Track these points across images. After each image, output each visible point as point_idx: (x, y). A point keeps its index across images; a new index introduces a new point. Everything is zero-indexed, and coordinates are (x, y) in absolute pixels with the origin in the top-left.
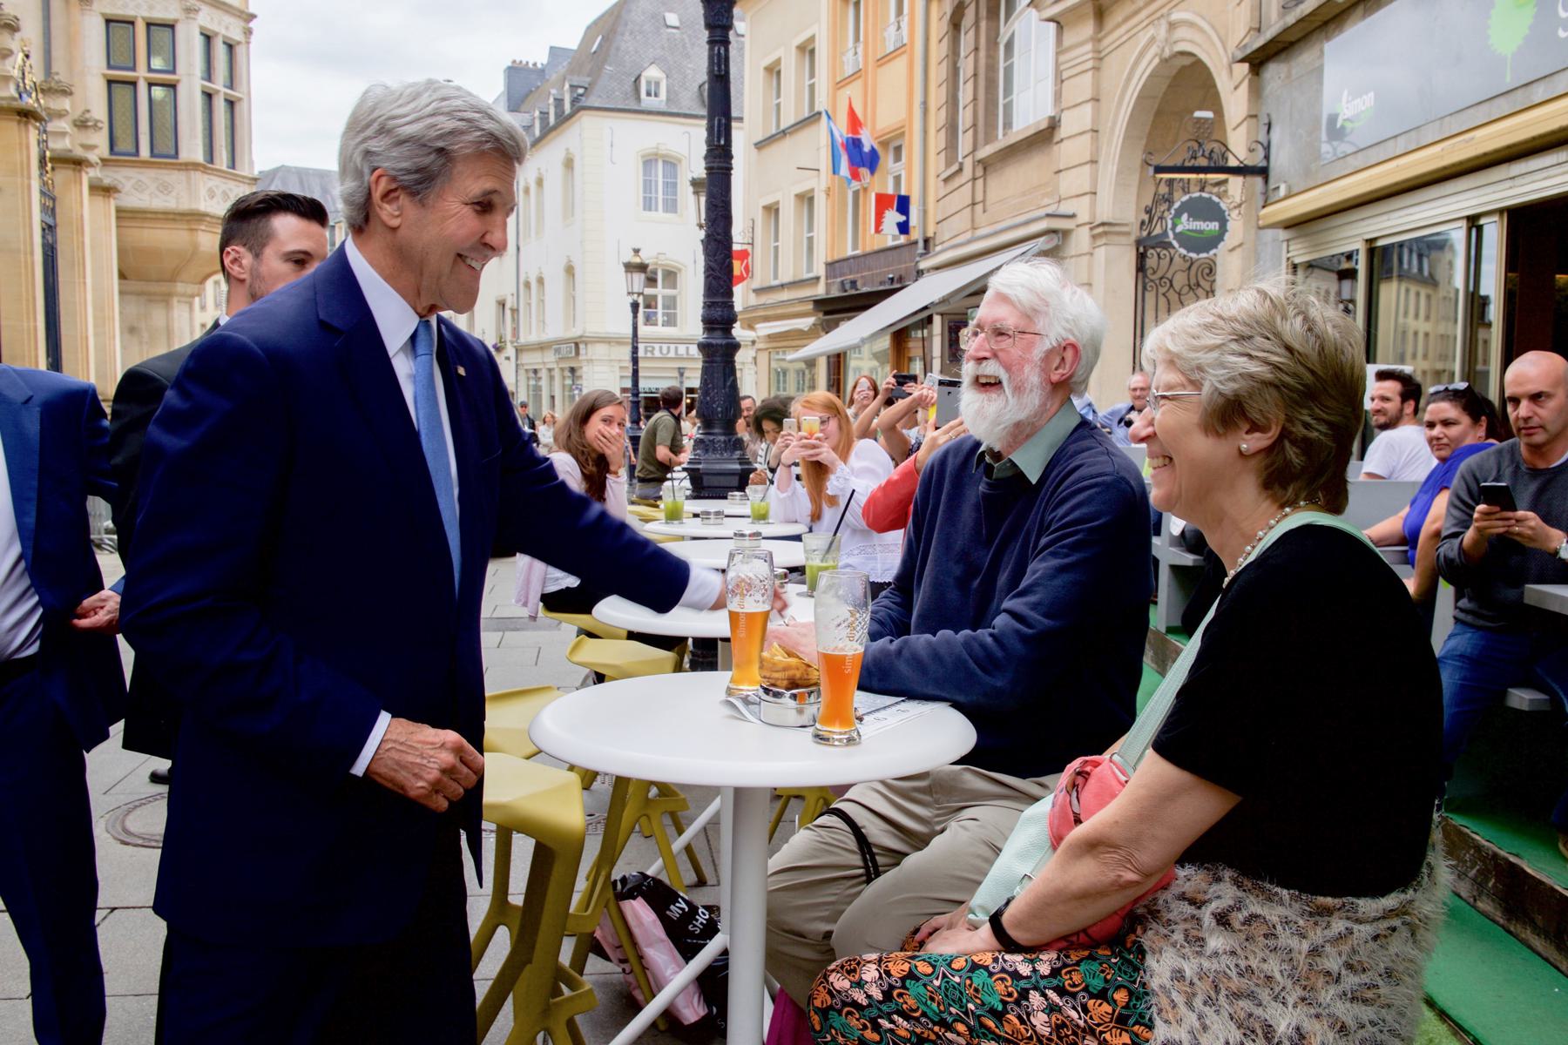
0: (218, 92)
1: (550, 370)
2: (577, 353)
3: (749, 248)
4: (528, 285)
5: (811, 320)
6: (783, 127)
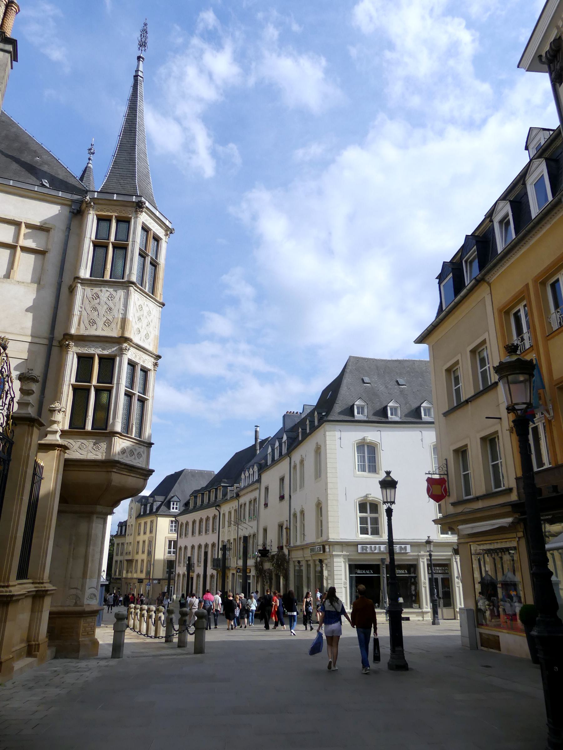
0: (134, 394)
1: (307, 561)
2: (324, 551)
3: (445, 477)
4: (295, 515)
5: (510, 520)
6: (463, 399)
